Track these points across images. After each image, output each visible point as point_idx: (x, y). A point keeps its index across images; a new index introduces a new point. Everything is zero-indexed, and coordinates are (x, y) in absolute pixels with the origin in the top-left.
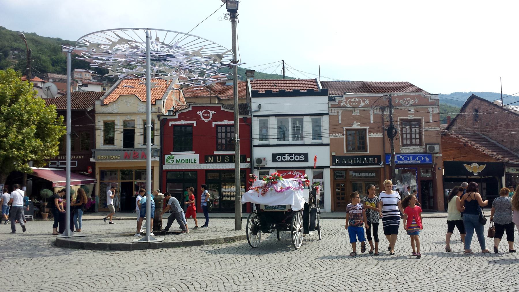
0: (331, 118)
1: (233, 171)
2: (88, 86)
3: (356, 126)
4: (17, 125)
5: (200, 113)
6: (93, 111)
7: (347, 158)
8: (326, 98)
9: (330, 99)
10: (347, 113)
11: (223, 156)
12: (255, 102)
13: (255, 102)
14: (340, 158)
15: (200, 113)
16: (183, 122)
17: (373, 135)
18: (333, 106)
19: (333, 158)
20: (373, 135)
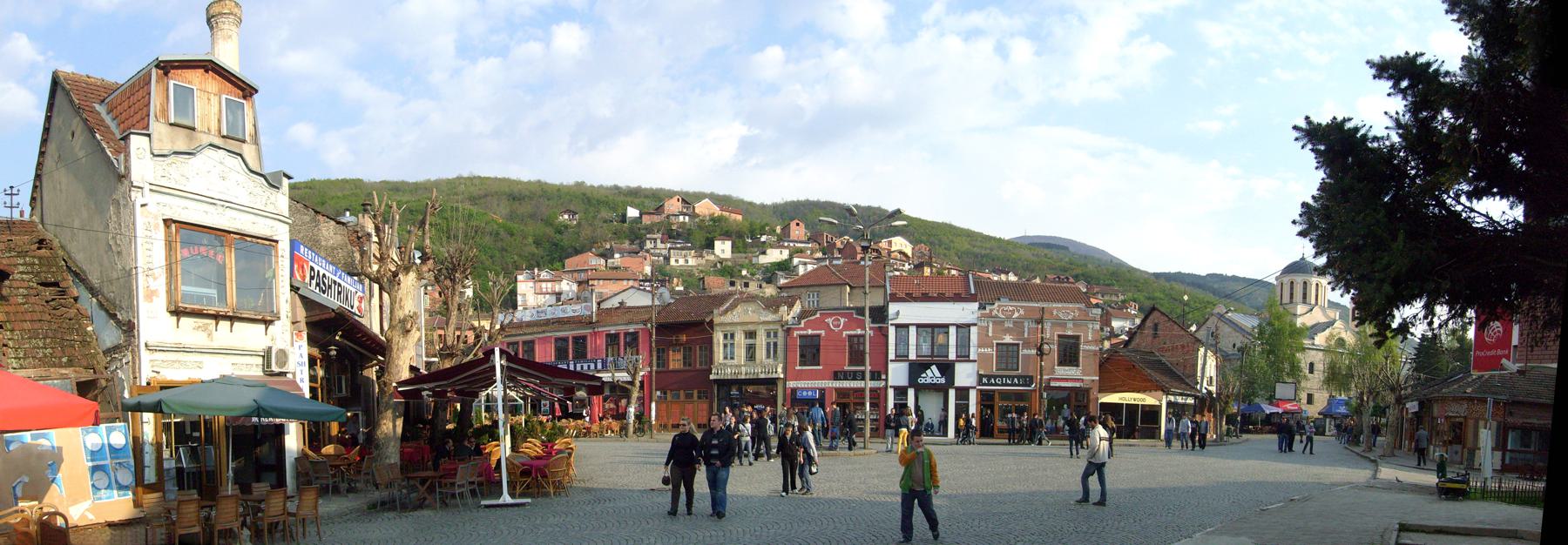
0: (981, 328)
1: (863, 390)
2: (1498, 454)
3: (1008, 339)
4: (672, 292)
5: (829, 320)
6: (711, 323)
7: (995, 377)
8: (976, 305)
9: (982, 307)
10: (998, 323)
11: (855, 372)
12: (893, 308)
13: (893, 308)
14: (989, 377)
15: (829, 320)
16: (810, 332)
17: (1026, 352)
18: (983, 316)
19: (980, 377)
20: (1026, 352)
